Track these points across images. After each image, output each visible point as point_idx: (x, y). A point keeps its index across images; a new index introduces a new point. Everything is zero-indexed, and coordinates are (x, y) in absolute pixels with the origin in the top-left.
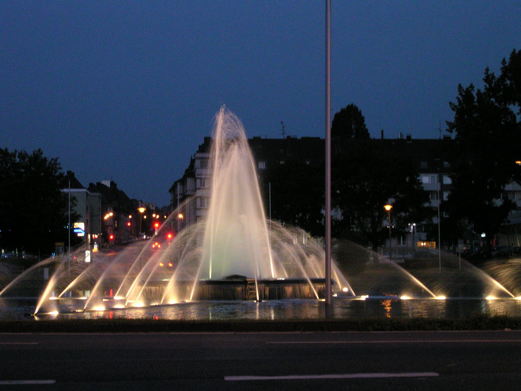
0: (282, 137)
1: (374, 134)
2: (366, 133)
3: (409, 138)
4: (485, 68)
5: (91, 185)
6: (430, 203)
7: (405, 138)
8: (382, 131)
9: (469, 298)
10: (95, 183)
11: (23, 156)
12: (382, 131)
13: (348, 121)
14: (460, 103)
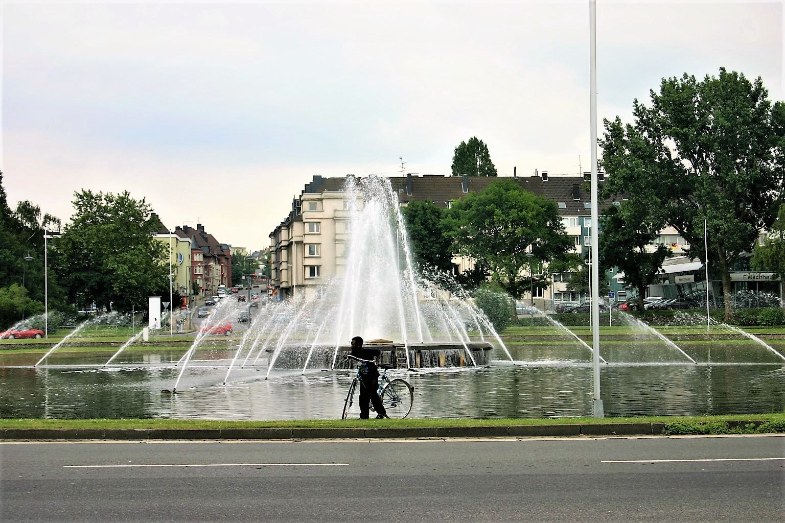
0: (400, 175)
1: (503, 170)
2: (492, 172)
3: (545, 175)
4: (633, 100)
5: (178, 228)
6: (575, 250)
7: (541, 175)
8: (515, 168)
9: (718, 364)
10: (182, 227)
11: (109, 199)
12: (515, 168)
13: (471, 155)
14: (608, 139)
